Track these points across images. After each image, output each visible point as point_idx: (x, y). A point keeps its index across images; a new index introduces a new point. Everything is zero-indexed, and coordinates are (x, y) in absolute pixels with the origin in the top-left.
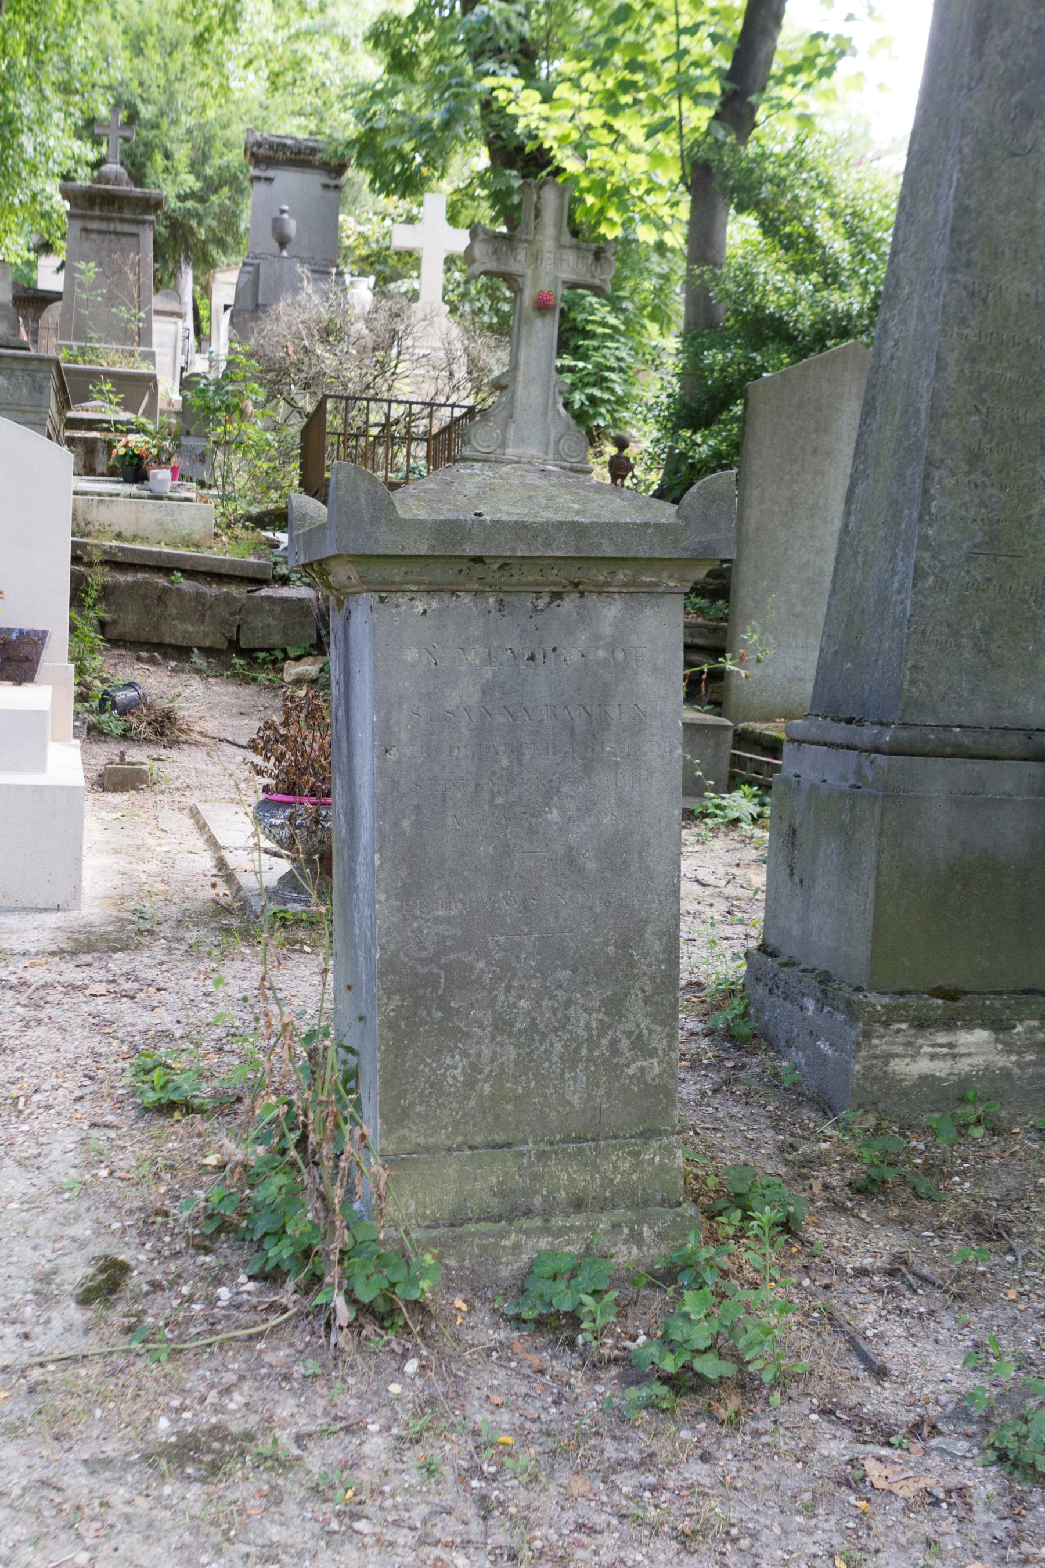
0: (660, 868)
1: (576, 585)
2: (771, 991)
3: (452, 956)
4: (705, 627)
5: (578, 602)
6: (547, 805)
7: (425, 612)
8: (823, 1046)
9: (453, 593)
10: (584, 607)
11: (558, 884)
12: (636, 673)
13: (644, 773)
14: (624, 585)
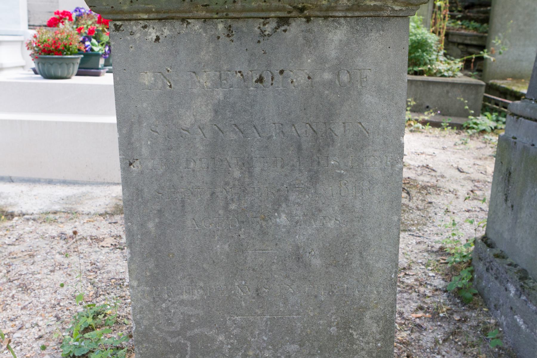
0: (379, 265)
1: (302, 10)
2: (487, 270)
3: (196, 331)
4: (477, 36)
5: (304, 27)
6: (276, 211)
7: (158, 39)
8: (520, 321)
9: (183, 20)
10: (309, 31)
11: (287, 277)
12: (360, 94)
13: (366, 183)
14: (349, 9)
